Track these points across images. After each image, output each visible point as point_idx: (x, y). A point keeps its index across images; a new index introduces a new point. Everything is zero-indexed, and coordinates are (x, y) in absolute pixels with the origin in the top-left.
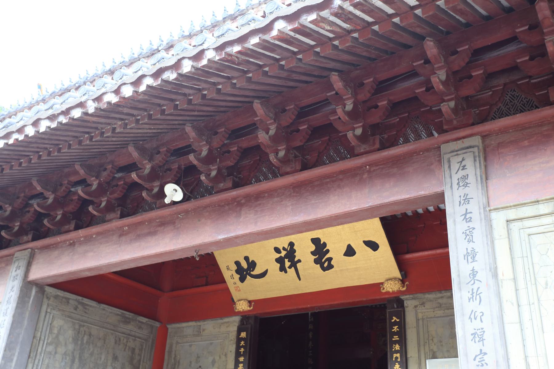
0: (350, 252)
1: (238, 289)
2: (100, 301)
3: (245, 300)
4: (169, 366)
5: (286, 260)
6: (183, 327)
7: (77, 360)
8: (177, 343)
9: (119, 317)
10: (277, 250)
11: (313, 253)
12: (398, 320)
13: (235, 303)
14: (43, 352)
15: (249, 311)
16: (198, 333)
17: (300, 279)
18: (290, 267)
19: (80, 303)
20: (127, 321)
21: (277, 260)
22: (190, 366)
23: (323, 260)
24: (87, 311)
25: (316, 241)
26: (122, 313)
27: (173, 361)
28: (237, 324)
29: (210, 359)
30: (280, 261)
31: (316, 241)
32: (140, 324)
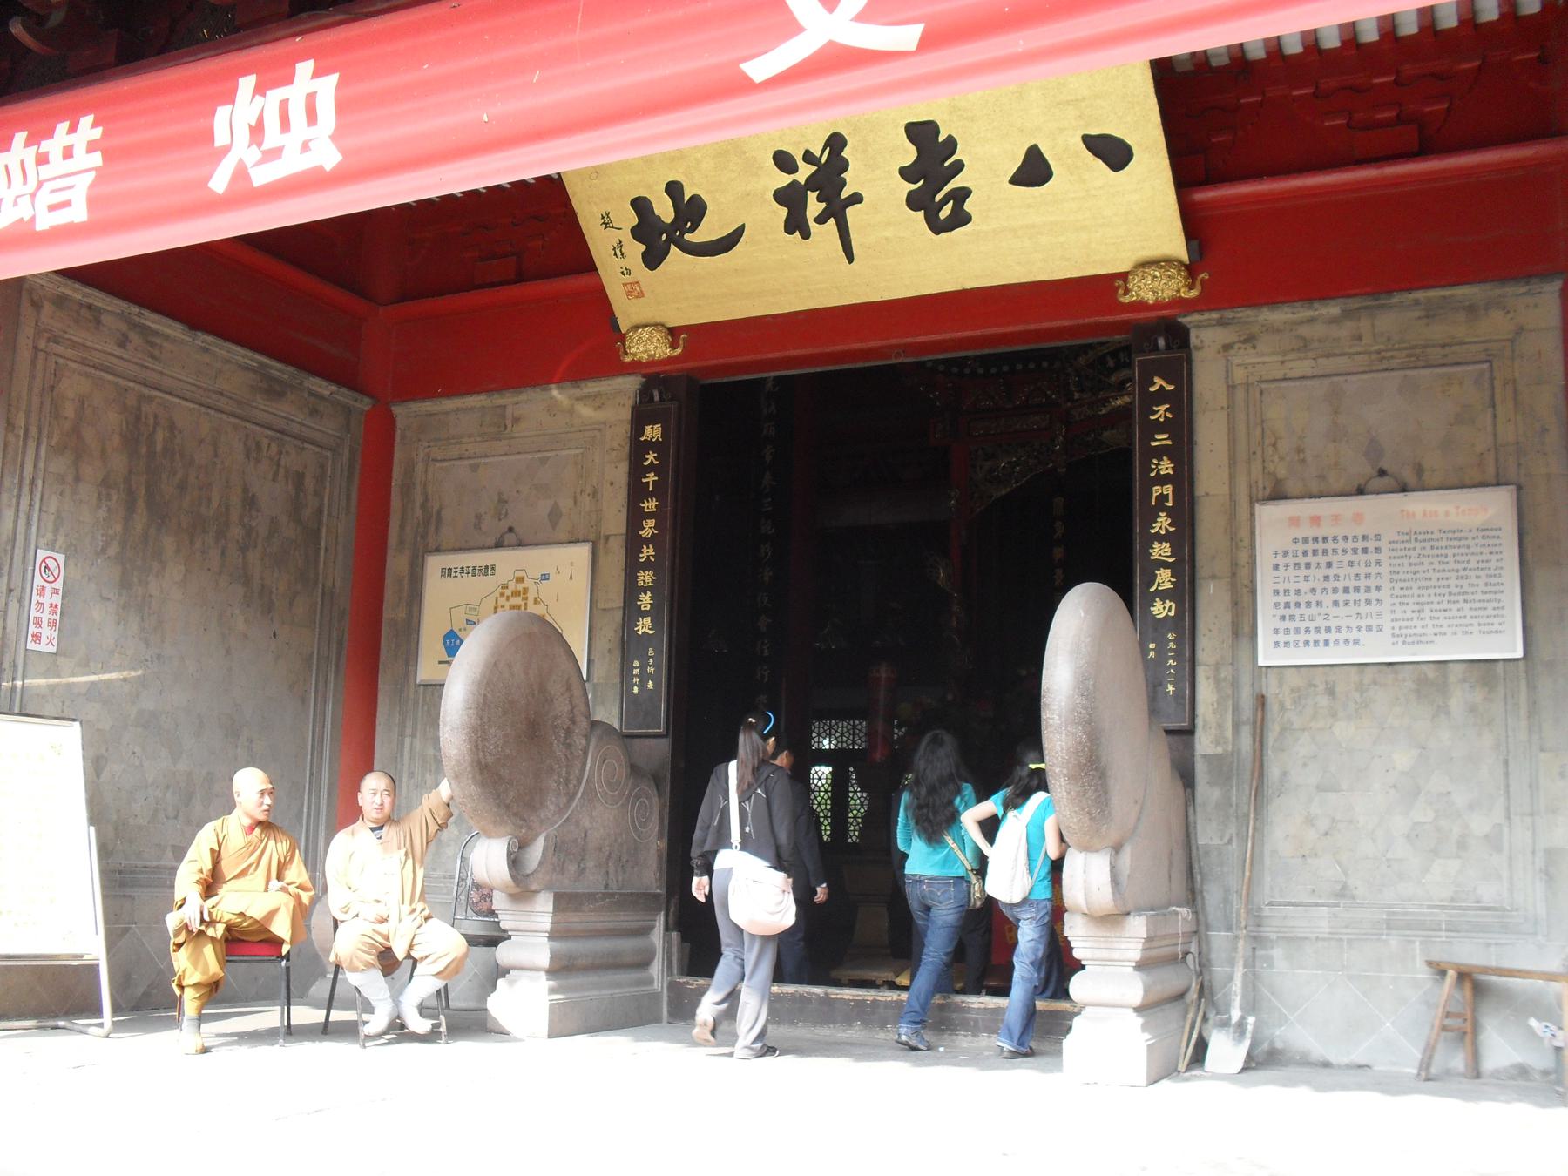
0: (1033, 171)
1: (634, 291)
2: (194, 324)
3: (656, 325)
4: (408, 529)
5: (812, 196)
6: (447, 413)
7: (141, 503)
8: (429, 459)
9: (251, 375)
10: (784, 161)
11: (906, 173)
12: (1170, 388)
13: (622, 337)
14: (41, 474)
15: (670, 360)
16: (500, 426)
17: (850, 259)
18: (821, 220)
19: (135, 326)
20: (274, 390)
21: (781, 196)
22: (477, 526)
23: (938, 198)
24: (156, 353)
25: (921, 133)
26: (261, 364)
27: (418, 512)
28: (630, 403)
29: (544, 507)
30: (790, 198)
31: (921, 133)
32: (312, 399)
